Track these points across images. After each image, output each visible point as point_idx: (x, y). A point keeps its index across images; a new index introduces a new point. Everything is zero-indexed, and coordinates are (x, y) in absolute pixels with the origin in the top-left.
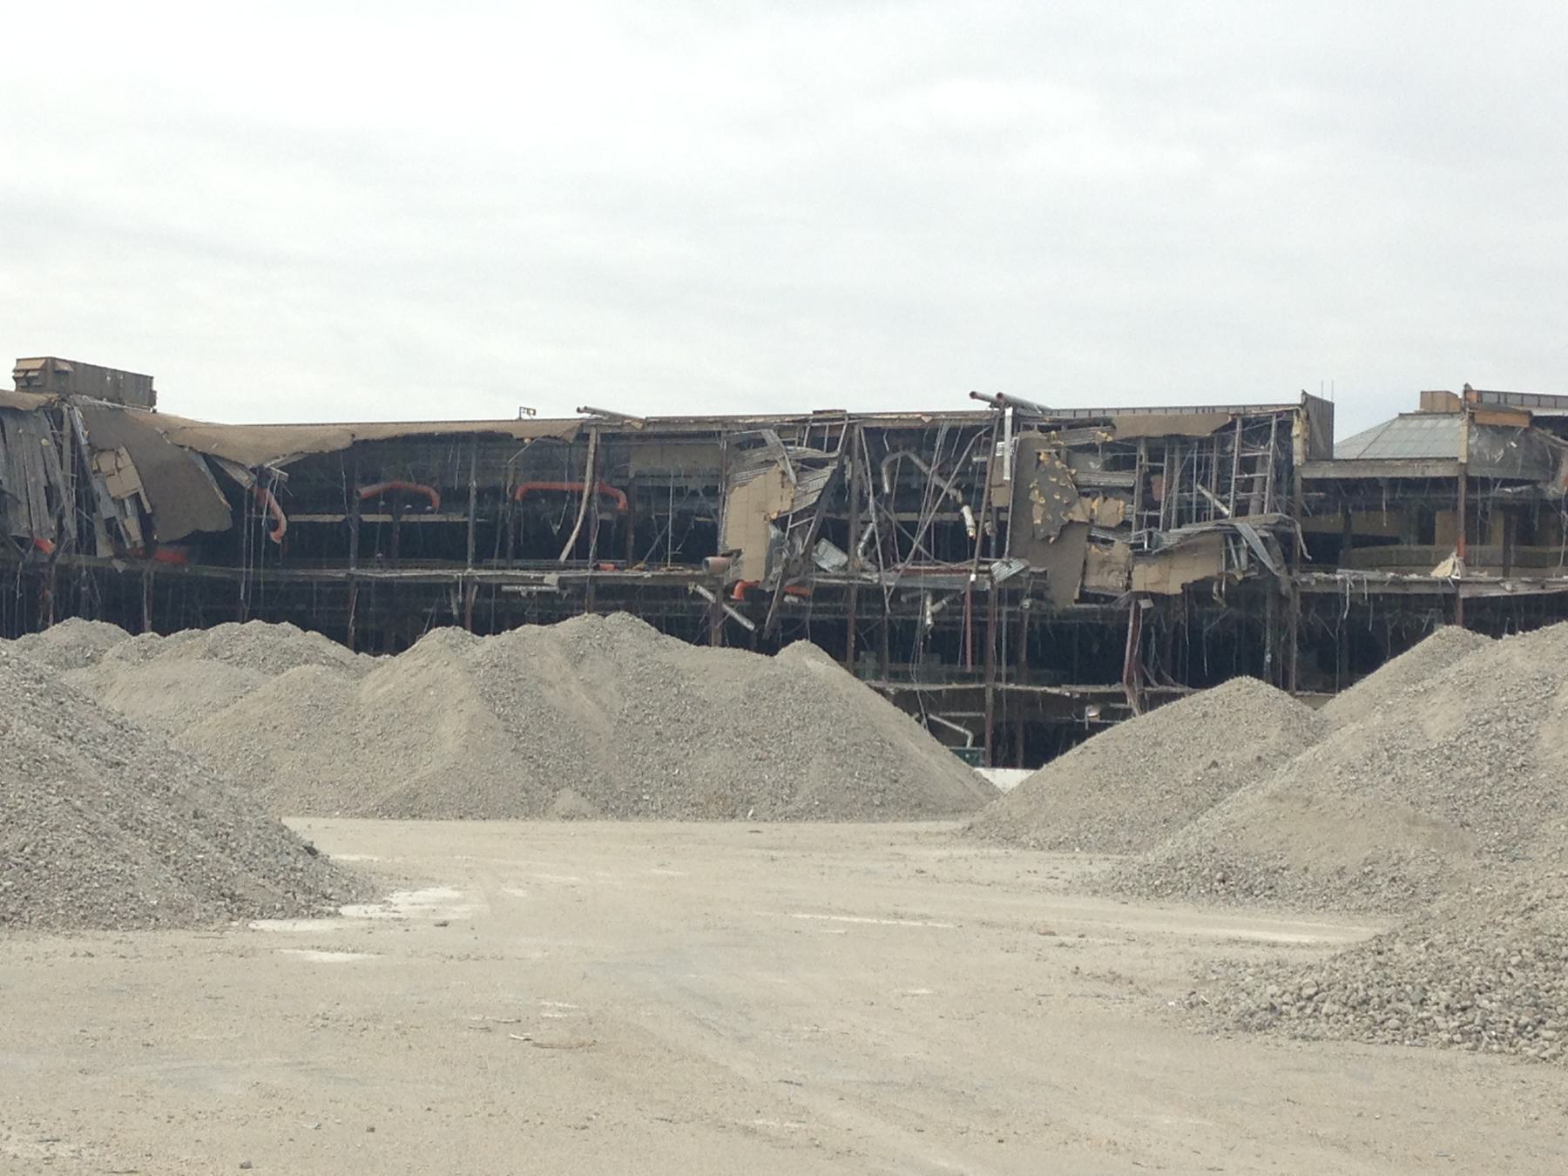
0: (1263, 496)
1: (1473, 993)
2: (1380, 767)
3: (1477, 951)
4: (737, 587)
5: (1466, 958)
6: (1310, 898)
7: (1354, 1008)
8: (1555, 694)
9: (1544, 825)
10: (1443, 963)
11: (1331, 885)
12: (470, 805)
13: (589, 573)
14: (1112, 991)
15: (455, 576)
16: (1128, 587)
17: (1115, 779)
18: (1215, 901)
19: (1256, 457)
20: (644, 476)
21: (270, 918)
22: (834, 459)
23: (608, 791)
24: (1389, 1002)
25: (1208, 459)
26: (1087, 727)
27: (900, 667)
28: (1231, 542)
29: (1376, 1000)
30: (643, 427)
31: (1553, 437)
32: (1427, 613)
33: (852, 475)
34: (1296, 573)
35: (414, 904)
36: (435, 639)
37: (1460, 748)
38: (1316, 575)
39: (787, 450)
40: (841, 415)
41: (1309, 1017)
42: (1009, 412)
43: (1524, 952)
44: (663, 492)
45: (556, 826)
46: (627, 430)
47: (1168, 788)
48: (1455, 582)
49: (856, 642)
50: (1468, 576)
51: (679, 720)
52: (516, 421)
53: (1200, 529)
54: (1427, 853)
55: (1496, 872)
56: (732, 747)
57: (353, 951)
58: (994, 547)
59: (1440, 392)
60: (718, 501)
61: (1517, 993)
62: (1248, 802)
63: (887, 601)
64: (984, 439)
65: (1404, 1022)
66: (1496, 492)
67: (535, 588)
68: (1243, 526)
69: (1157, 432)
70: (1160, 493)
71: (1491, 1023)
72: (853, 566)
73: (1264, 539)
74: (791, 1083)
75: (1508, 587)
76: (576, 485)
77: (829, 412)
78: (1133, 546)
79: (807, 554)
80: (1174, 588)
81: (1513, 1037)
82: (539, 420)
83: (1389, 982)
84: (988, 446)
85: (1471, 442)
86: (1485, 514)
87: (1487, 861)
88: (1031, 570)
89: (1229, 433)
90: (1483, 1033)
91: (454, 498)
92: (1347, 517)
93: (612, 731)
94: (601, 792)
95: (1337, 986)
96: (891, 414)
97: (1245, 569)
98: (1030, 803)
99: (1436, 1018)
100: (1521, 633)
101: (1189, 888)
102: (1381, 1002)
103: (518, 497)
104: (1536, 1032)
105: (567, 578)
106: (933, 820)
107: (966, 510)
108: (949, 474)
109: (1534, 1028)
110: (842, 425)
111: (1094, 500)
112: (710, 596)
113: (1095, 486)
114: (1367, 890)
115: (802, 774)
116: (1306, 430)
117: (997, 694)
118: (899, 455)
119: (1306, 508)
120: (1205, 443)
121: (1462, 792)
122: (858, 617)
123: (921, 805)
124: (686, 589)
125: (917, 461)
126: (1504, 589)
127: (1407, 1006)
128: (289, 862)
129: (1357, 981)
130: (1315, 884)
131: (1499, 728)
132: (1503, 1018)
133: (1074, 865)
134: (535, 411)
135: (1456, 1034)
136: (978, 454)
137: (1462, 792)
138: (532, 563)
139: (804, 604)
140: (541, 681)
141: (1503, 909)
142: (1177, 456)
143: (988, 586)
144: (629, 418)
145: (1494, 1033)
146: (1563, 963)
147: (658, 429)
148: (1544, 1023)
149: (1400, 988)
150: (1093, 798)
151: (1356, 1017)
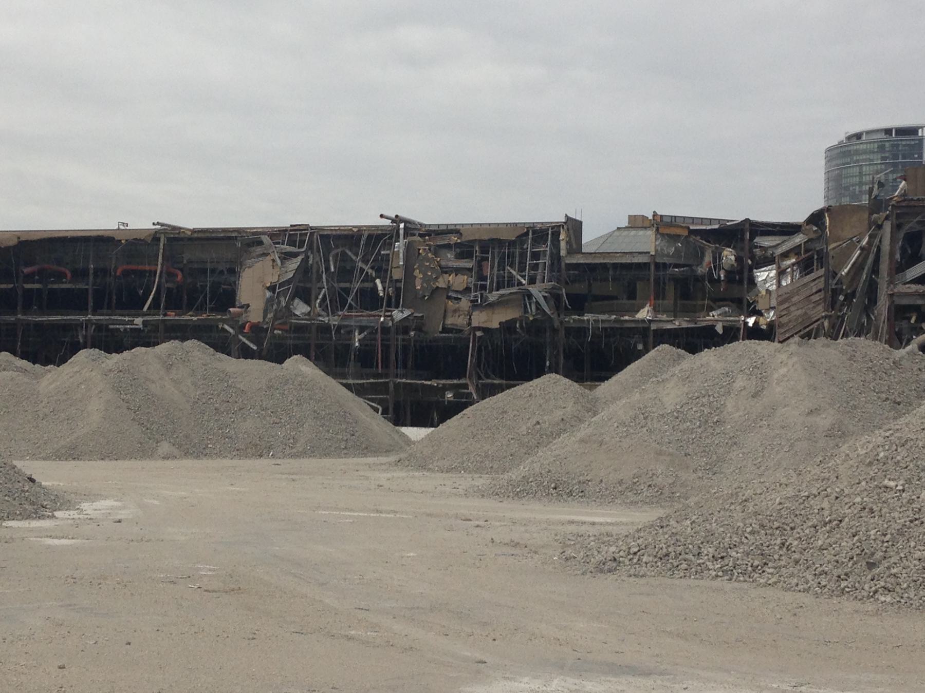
0: (545, 273)
1: (727, 549)
2: (640, 423)
3: (728, 525)
4: (247, 325)
5: (722, 529)
6: (604, 497)
7: (661, 559)
8: (734, 382)
9: (730, 454)
10: (709, 532)
11: (616, 490)
12: (107, 452)
13: (161, 317)
14: (517, 551)
15: (81, 320)
16: (469, 324)
17: (481, 432)
18: (552, 500)
19: (540, 251)
20: (191, 262)
21: (13, 519)
22: (303, 252)
23: (188, 443)
24: (680, 554)
25: (513, 253)
26: (446, 403)
27: (338, 370)
28: (526, 299)
29: (673, 553)
30: (191, 234)
31: (701, 241)
32: (633, 338)
33: (313, 262)
34: (562, 316)
35: (96, 510)
36: (83, 355)
37: (683, 412)
38: (573, 317)
39: (276, 247)
40: (307, 227)
41: (636, 564)
42: (402, 226)
43: (753, 525)
44: (204, 271)
45: (160, 463)
46: (182, 235)
47: (512, 437)
48: (648, 320)
49: (315, 356)
50: (656, 317)
51: (228, 402)
52: (116, 230)
53: (510, 291)
54: (668, 471)
55: (706, 481)
56: (259, 417)
57: (73, 538)
58: (393, 302)
59: (640, 216)
60: (236, 276)
61: (751, 548)
62: (566, 443)
63: (333, 333)
64: (388, 241)
65: (689, 565)
66: (671, 271)
67: (128, 326)
68: (534, 290)
69: (486, 237)
70: (487, 272)
71: (738, 565)
72: (314, 313)
73: (545, 297)
74: (362, 609)
75: (677, 323)
76: (153, 268)
77: (299, 225)
78: (472, 301)
79: (287, 307)
80: (495, 325)
81: (751, 573)
82: (130, 230)
83: (679, 543)
84: (390, 245)
85: (657, 243)
86: (664, 283)
87: (700, 474)
88: (415, 315)
89: (524, 238)
90: (734, 570)
91: (79, 274)
92: (590, 285)
93: (190, 408)
94: (184, 443)
95: (650, 547)
96: (335, 227)
97: (534, 314)
98: (433, 446)
99: (708, 563)
100: (714, 348)
101: (536, 493)
102: (676, 554)
103: (118, 274)
104: (763, 569)
105: (147, 320)
106: (375, 456)
107: (378, 281)
108: (368, 261)
109: (762, 567)
110: (307, 233)
111: (450, 275)
112: (231, 330)
113: (450, 268)
114: (635, 492)
115: (300, 432)
116: (567, 236)
117: (397, 386)
118: (339, 250)
119: (567, 279)
120: (512, 243)
121: (685, 437)
122: (317, 342)
123: (366, 448)
124: (218, 326)
125: (350, 253)
126: (675, 324)
127: (690, 557)
128: (20, 486)
129: (661, 544)
130: (607, 489)
131: (704, 401)
132: (745, 562)
133: (465, 481)
134: (127, 224)
135: (719, 572)
136: (384, 250)
137: (685, 437)
138: (126, 312)
139: (285, 335)
140: (147, 379)
141: (730, 501)
142: (496, 251)
143: (390, 324)
144: (183, 228)
145: (740, 571)
146: (775, 531)
147: (200, 235)
148: (767, 564)
149: (686, 547)
150: (469, 443)
151: (662, 563)
